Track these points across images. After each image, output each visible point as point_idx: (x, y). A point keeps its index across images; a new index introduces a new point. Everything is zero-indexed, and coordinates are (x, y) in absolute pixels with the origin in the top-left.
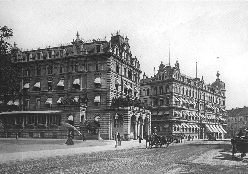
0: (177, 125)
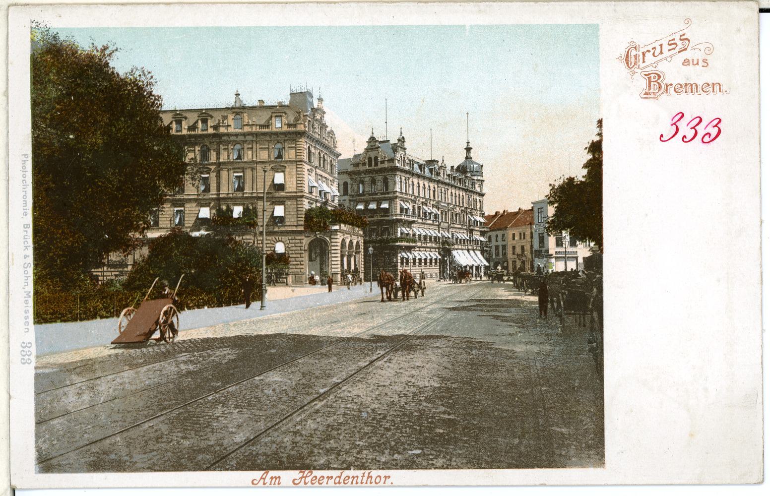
0: (406, 253)
